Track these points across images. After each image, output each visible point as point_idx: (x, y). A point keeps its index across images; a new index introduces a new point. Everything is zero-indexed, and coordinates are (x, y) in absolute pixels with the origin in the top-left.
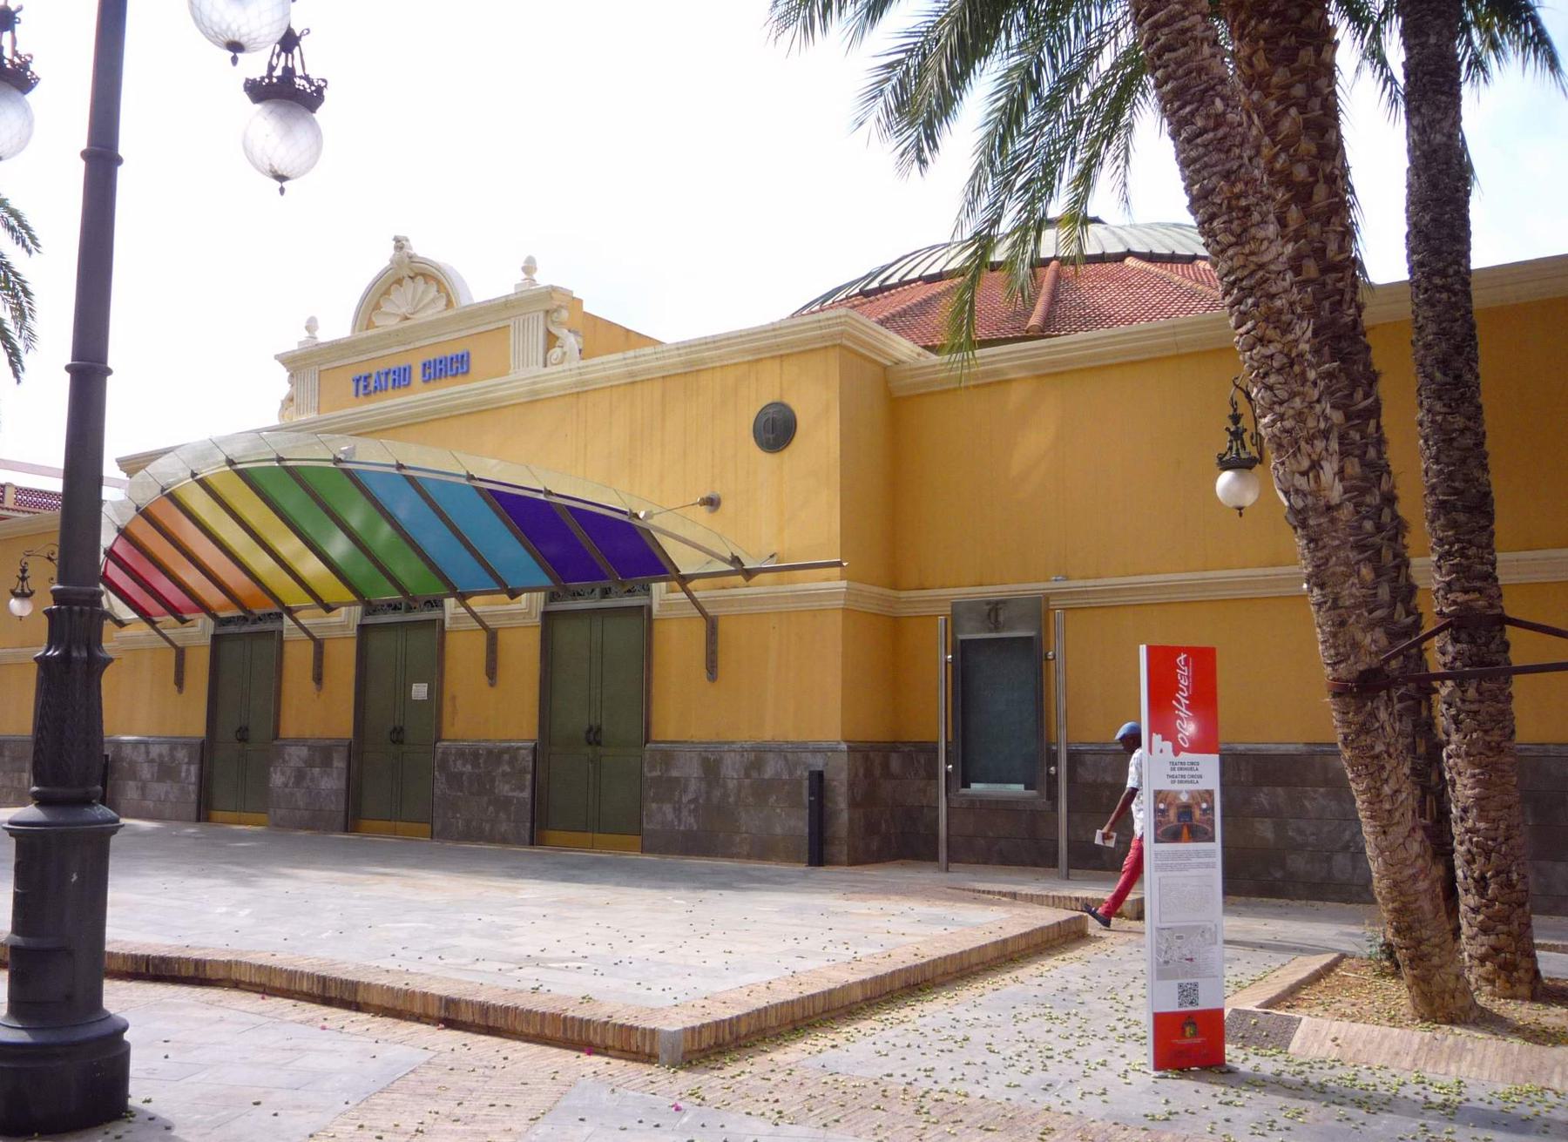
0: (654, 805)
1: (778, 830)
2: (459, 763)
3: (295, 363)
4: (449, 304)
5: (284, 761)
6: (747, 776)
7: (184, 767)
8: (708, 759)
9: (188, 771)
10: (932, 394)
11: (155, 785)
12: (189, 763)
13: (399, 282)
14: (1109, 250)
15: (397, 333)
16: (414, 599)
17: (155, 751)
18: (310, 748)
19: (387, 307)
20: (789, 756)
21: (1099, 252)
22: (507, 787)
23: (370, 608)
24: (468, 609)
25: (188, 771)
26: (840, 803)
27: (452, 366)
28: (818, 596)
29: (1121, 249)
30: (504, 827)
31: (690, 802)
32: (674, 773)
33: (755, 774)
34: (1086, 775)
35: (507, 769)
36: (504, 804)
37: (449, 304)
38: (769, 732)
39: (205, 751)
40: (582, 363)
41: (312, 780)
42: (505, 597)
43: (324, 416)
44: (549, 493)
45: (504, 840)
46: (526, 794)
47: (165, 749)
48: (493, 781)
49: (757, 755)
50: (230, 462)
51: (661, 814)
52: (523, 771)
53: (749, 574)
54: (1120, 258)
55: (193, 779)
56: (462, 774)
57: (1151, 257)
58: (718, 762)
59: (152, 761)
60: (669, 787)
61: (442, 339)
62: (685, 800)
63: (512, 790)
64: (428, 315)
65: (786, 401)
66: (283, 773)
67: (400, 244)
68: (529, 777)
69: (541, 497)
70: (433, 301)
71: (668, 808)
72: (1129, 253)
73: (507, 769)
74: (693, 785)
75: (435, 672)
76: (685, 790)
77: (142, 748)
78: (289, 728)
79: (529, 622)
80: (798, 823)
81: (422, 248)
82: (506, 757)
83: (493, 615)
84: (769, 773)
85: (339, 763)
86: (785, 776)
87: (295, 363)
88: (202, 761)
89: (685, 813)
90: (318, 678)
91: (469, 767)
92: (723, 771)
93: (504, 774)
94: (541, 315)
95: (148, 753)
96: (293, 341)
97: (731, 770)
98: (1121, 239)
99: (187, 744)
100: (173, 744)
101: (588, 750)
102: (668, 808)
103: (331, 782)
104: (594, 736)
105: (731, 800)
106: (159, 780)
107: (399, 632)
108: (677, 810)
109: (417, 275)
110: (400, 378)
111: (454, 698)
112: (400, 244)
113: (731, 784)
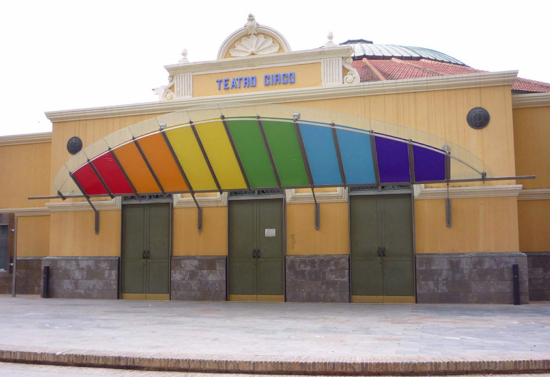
0: (423, 282)
1: (493, 290)
2: (302, 266)
3: (174, 72)
4: (281, 49)
5: (181, 267)
6: (475, 267)
7: (107, 272)
8: (453, 261)
9: (110, 275)
10: (525, 108)
11: (84, 281)
12: (111, 269)
13: (248, 35)
14: (376, 54)
15: (248, 61)
16: (165, 193)
17: (83, 264)
18: (199, 260)
19: (238, 47)
20: (497, 259)
21: (372, 55)
22: (334, 276)
23: (352, 188)
24: (90, 203)
25: (110, 275)
26: (525, 277)
27: (288, 79)
28: (507, 191)
29: (391, 55)
30: (333, 295)
31: (443, 280)
32: (434, 268)
33: (478, 267)
34: (283, 296)
35: (333, 268)
36: (333, 284)
37: (281, 49)
38: (481, 248)
39: (120, 264)
40: (362, 84)
41: (202, 276)
42: (61, 199)
43: (194, 99)
44: (411, 141)
45: (333, 301)
46: (346, 279)
47: (91, 263)
48: (324, 273)
49: (479, 260)
50: (223, 117)
51: (426, 287)
52: (344, 268)
53: (64, 198)
54: (389, 58)
55: (114, 278)
56: (304, 271)
57: (402, 58)
58: (458, 263)
59: (82, 269)
60: (430, 275)
61: (275, 65)
62: (440, 279)
63: (337, 278)
64: (267, 53)
65: (484, 107)
66: (181, 273)
67: (251, 18)
68: (347, 271)
69: (407, 142)
70: (270, 47)
71: (431, 284)
72: (393, 56)
73: (333, 268)
74: (444, 273)
75: (281, 226)
76: (440, 274)
77: (74, 263)
78: (179, 250)
79: (340, 200)
80: (507, 287)
81: (262, 21)
82: (333, 262)
83: (99, 205)
84: (486, 266)
85: (221, 268)
86: (495, 267)
87: (174, 72)
88: (119, 268)
89: (441, 285)
90: (200, 227)
91: (308, 268)
92: (461, 266)
93: (331, 270)
94: (341, 59)
95: (78, 265)
96: (175, 60)
97: (465, 266)
98: (372, 51)
99: (107, 260)
100: (97, 260)
101: (379, 258)
102: (431, 284)
103: (216, 277)
104: (382, 253)
105: (467, 278)
106: (87, 279)
107: (255, 205)
108: (436, 284)
109: (259, 34)
110: (250, 83)
111: (293, 236)
112: (251, 18)
113: (465, 272)
